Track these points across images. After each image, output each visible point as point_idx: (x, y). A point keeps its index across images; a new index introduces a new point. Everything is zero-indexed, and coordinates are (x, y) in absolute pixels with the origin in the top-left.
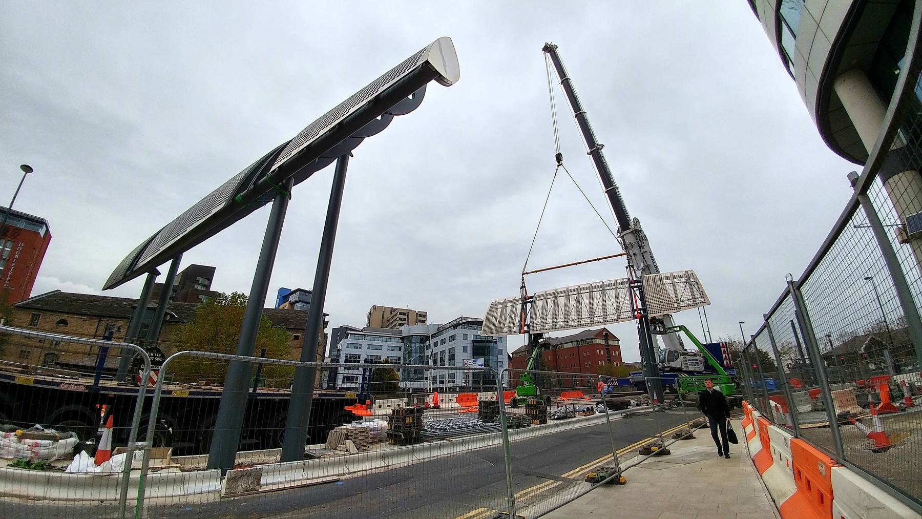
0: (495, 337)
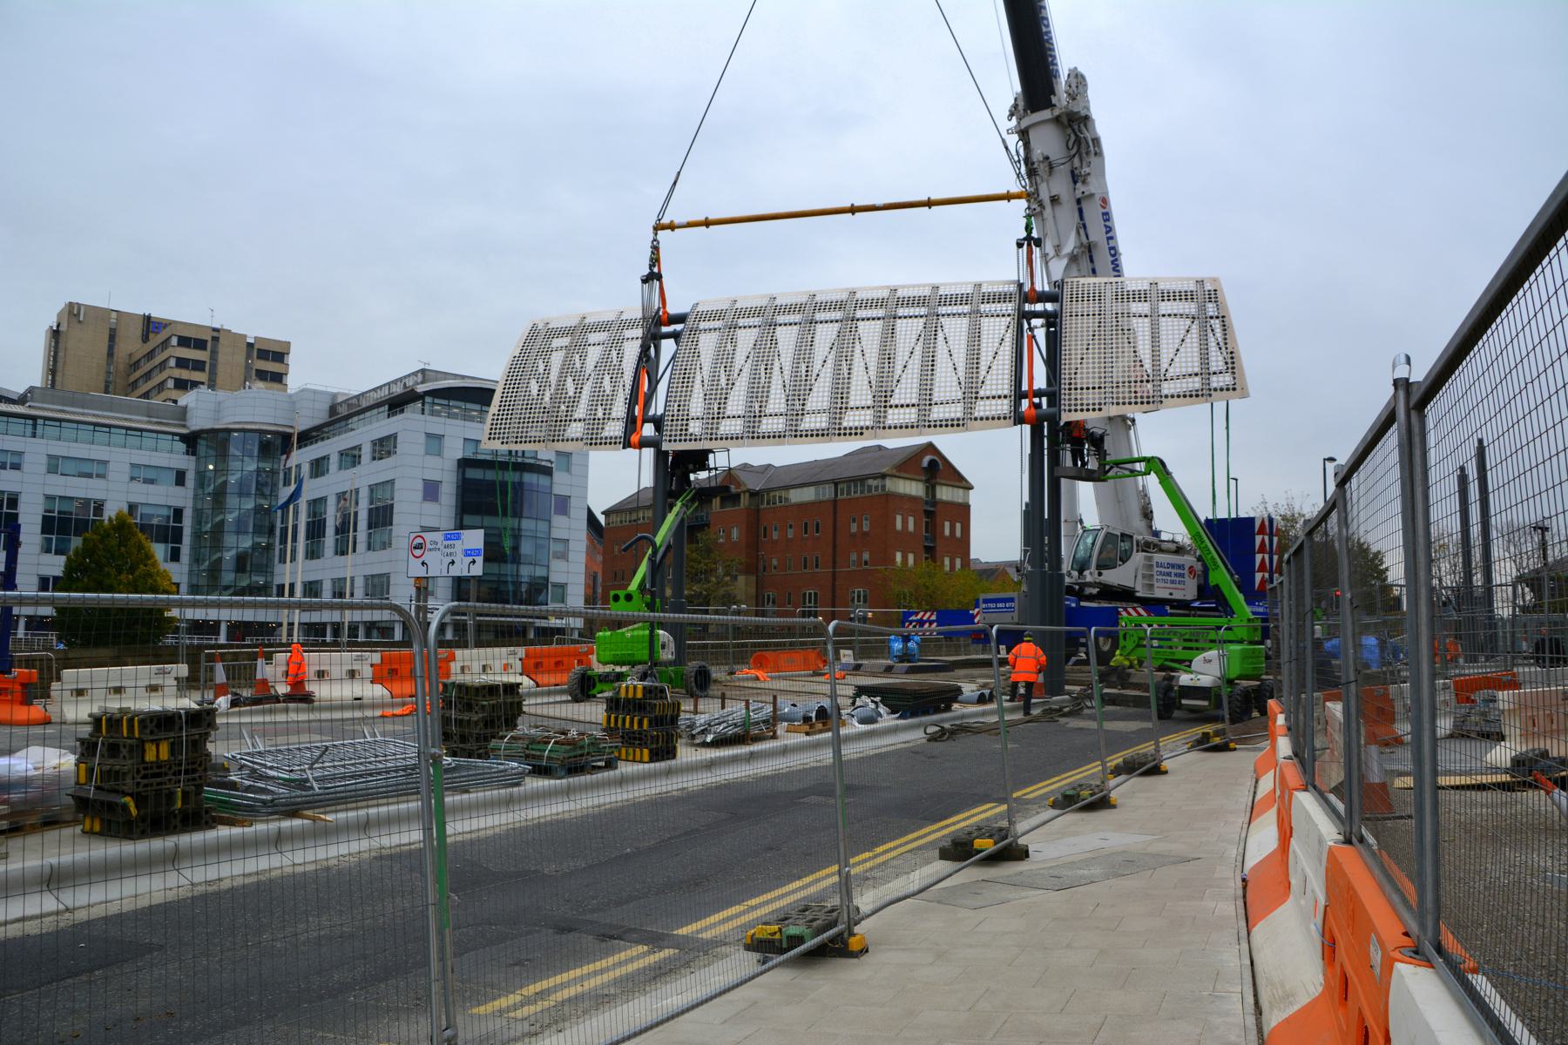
0: (545, 453)
